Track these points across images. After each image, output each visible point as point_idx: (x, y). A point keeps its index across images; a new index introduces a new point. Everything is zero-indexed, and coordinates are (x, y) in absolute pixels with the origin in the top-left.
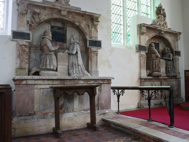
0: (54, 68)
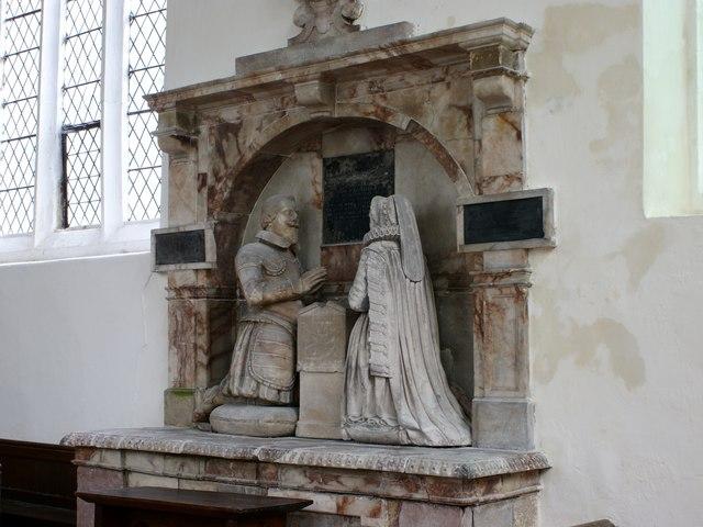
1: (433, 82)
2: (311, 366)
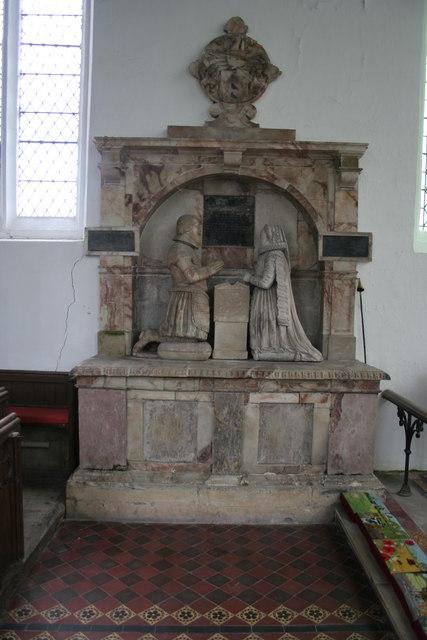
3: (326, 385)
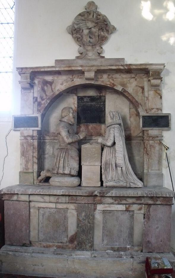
0: (70, 172)
1: (131, 78)
2: (85, 164)
3: (141, 200)
